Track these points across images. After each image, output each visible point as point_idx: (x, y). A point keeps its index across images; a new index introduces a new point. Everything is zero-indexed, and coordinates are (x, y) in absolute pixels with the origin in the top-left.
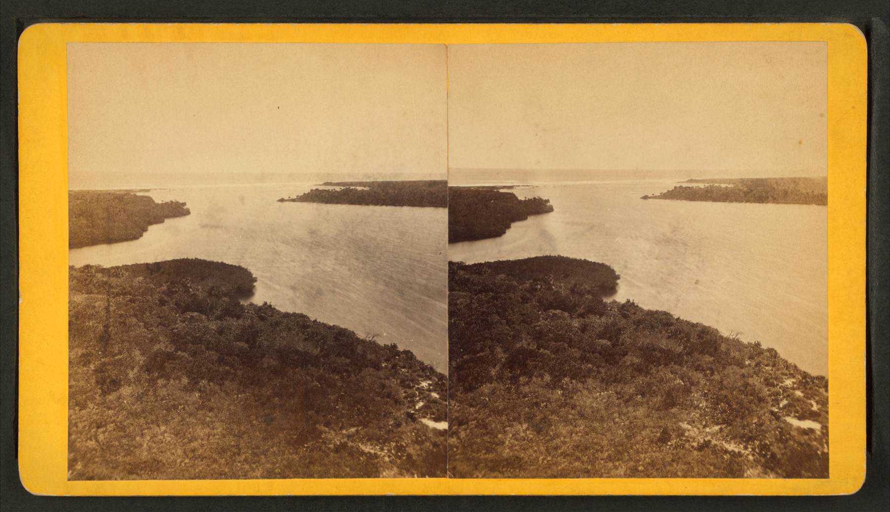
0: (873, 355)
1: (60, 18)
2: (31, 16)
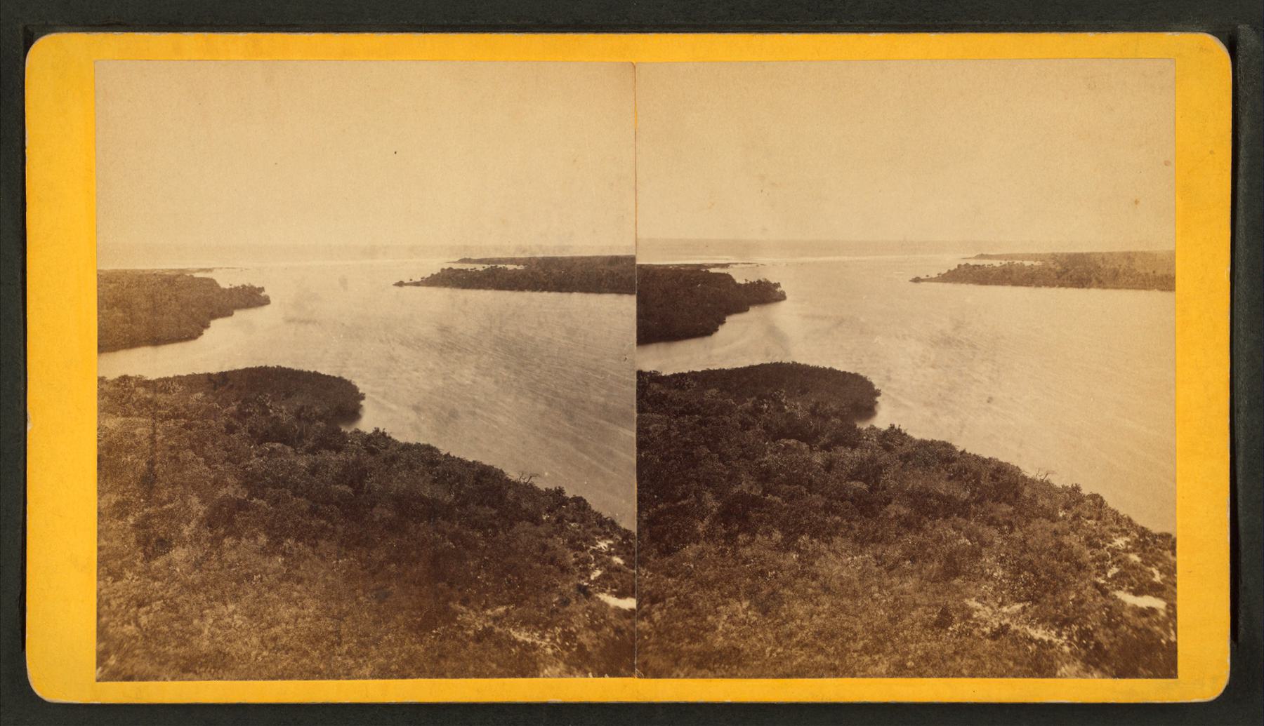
1: (85, 25)
2: (44, 22)
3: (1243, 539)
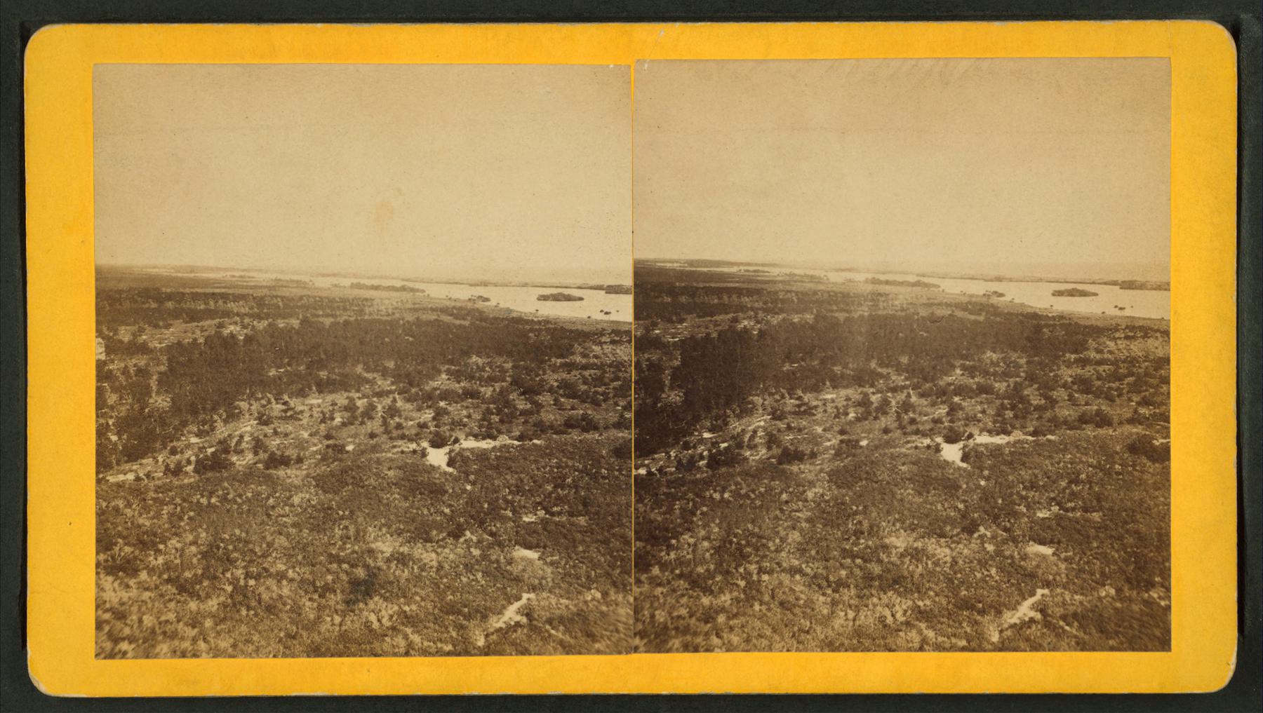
0: (1246, 496)
3: (1248, 530)
